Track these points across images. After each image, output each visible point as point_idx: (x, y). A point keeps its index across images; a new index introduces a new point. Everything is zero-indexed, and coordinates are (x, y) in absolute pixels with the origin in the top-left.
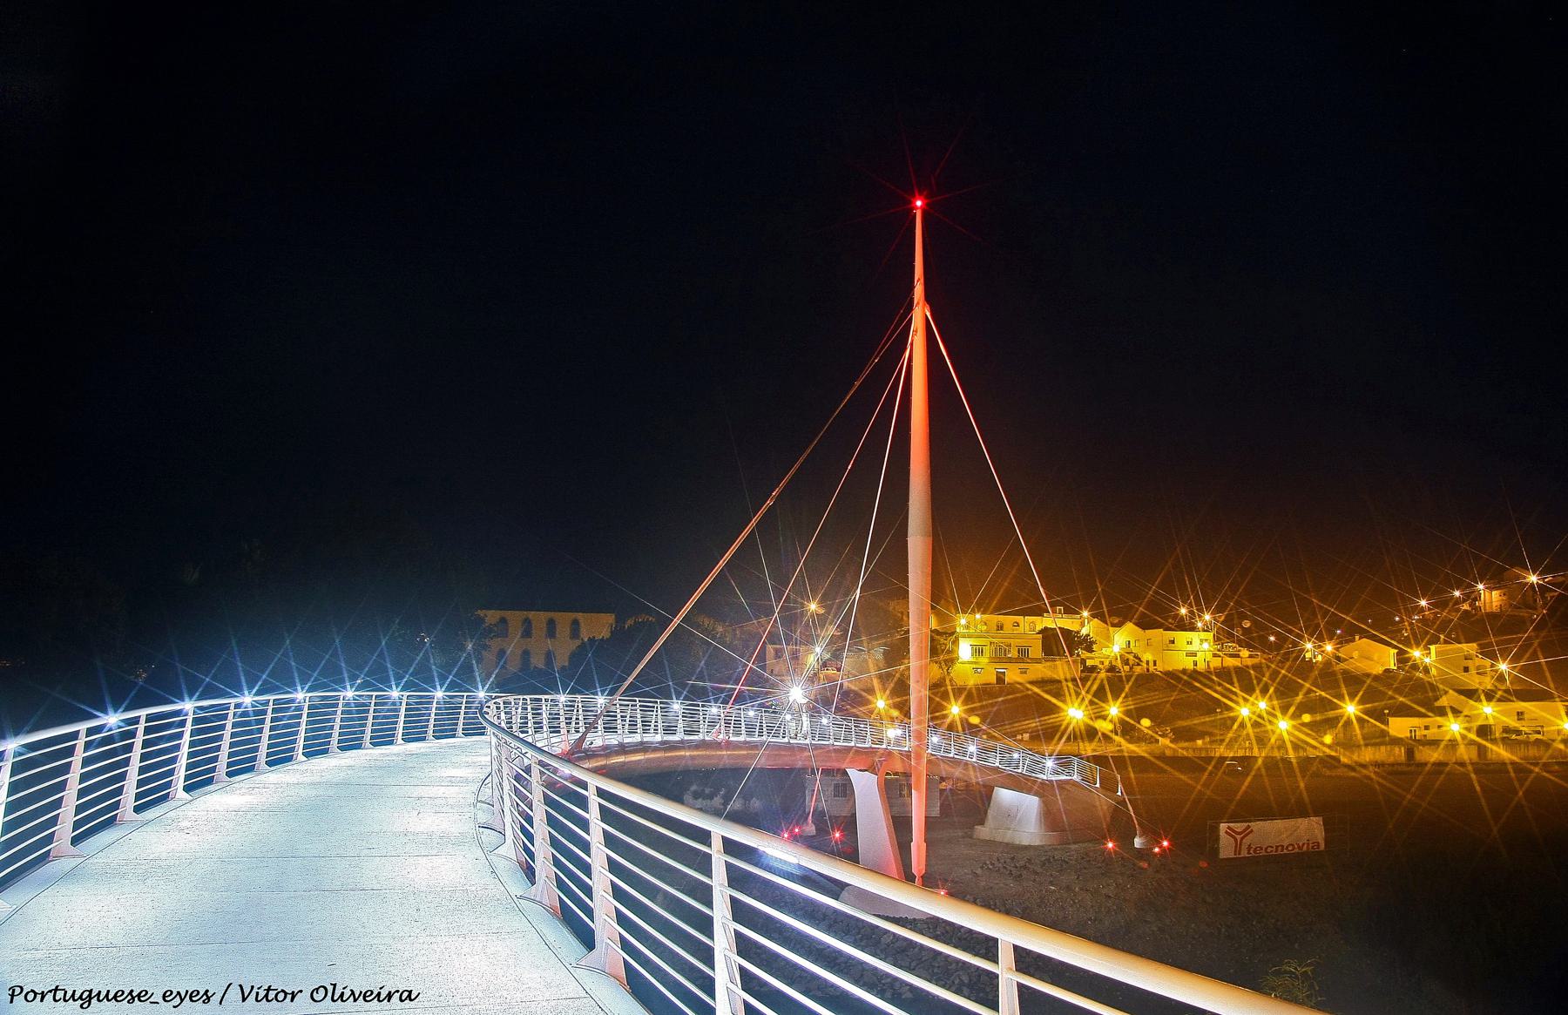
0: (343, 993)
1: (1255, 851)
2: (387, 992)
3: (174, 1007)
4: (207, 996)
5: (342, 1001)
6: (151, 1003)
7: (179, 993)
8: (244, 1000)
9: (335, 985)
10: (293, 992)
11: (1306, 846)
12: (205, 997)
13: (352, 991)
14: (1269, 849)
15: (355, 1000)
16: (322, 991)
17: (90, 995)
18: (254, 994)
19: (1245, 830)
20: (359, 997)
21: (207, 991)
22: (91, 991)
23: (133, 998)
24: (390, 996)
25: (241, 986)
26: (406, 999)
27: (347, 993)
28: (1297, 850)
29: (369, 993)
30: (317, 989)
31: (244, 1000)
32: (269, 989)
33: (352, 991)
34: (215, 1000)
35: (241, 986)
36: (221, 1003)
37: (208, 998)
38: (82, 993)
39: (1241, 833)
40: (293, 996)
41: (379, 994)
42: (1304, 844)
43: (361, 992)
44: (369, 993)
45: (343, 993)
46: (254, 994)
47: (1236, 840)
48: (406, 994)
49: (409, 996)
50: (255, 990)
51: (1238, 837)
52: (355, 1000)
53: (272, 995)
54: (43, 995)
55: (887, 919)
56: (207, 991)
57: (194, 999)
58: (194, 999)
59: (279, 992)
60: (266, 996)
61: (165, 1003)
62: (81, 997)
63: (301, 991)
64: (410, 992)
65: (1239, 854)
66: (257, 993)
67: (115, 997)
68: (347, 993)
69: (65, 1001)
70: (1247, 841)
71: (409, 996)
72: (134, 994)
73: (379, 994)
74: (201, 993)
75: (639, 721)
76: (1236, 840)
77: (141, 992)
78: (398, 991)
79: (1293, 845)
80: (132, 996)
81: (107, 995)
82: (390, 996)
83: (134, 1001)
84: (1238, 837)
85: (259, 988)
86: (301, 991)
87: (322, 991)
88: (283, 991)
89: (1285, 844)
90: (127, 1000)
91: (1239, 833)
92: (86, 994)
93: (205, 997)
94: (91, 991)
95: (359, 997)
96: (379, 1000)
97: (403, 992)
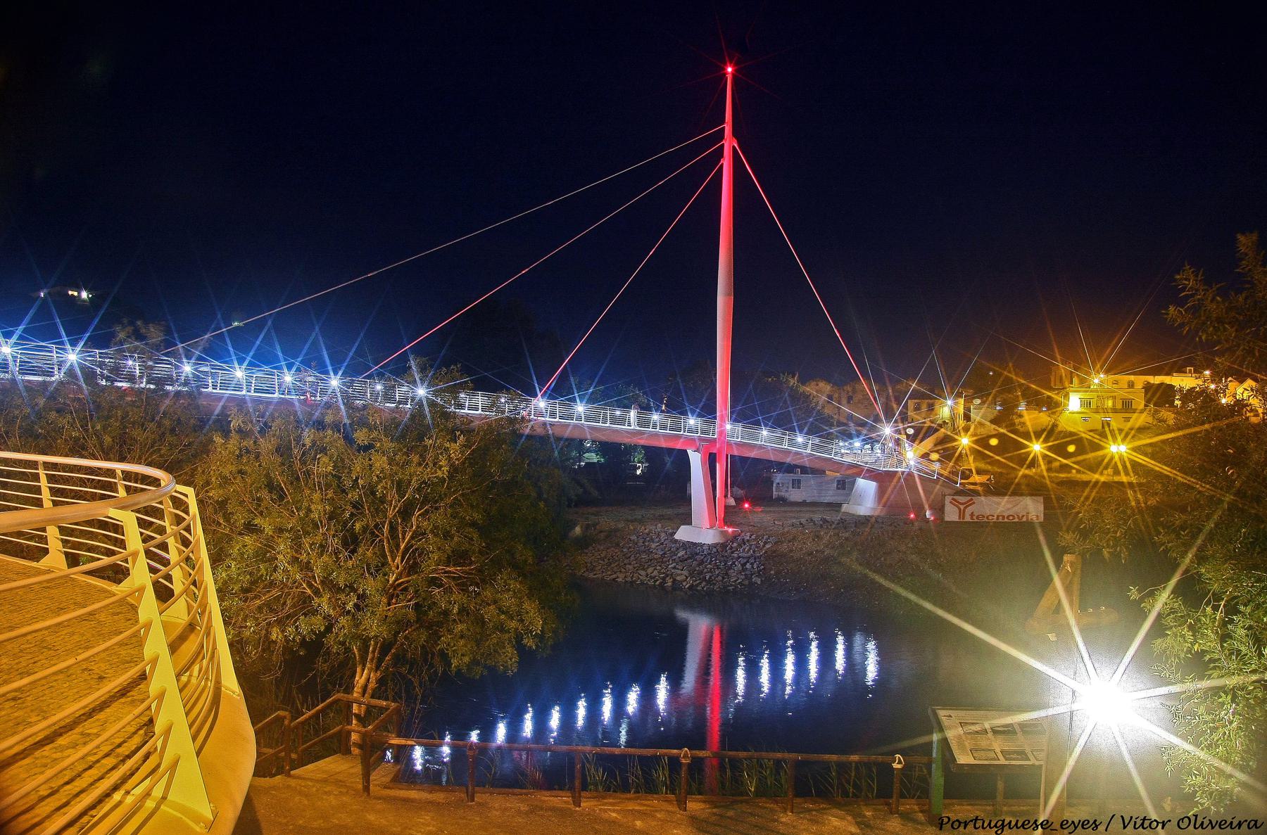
0: (1203, 822)
1: (978, 517)
2: (1237, 823)
3: (1070, 833)
4: (1096, 824)
5: (1202, 828)
6: (1051, 830)
7: (1073, 822)
8: (1125, 827)
9: (1196, 816)
10: (1164, 822)
11: (1025, 517)
12: (1034, 825)
13: (1210, 820)
14: (990, 518)
15: (1213, 828)
16: (1186, 820)
17: (1003, 824)
18: (1132, 823)
19: (968, 502)
20: (1128, 824)
21: (1096, 821)
22: (1003, 821)
23: (1037, 827)
24: (1240, 824)
25: (1122, 817)
26: (1235, 827)
27: (1206, 822)
28: (1016, 520)
29: (1086, 822)
30: (1183, 819)
31: (1125, 827)
32: (1144, 819)
33: (1210, 820)
34: (1101, 828)
35: (1122, 817)
36: (1106, 830)
37: (1097, 826)
38: (997, 823)
39: (965, 503)
40: (1164, 824)
41: (1231, 823)
42: (1023, 516)
43: (1217, 822)
44: (1086, 822)
45: (1203, 822)
46: (1132, 823)
47: (960, 509)
48: (1253, 823)
49: (1255, 824)
50: (1134, 820)
51: (962, 507)
52: (1213, 828)
53: (1147, 824)
54: (966, 824)
55: (27, 509)
56: (1096, 821)
57: (1222, 827)
58: (1222, 827)
59: (1152, 822)
60: (1142, 824)
61: (1083, 830)
62: (995, 826)
63: (1170, 821)
64: (1256, 821)
65: (963, 519)
66: (1135, 822)
67: (1023, 825)
68: (1206, 822)
69: (983, 828)
70: (968, 511)
71: (1255, 824)
72: (1039, 823)
73: (1231, 823)
74: (1091, 823)
75: (533, 413)
76: (960, 509)
77: (1222, 821)
78: (1246, 821)
79: (1013, 516)
80: (1036, 824)
81: (989, 824)
82: (1240, 824)
83: (1037, 828)
84: (962, 507)
85: (1136, 819)
86: (1170, 821)
87: (1186, 820)
88: (1155, 820)
89: (1006, 515)
90: (1032, 827)
91: (962, 504)
92: (1000, 823)
93: (1094, 825)
94: (1256, 821)
95: (1128, 824)
96: (1231, 828)
97: (1251, 821)
